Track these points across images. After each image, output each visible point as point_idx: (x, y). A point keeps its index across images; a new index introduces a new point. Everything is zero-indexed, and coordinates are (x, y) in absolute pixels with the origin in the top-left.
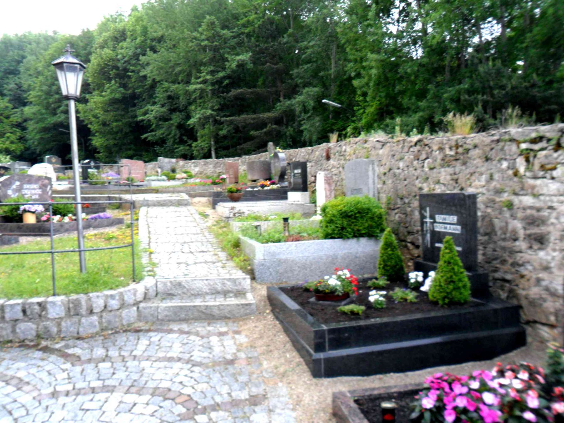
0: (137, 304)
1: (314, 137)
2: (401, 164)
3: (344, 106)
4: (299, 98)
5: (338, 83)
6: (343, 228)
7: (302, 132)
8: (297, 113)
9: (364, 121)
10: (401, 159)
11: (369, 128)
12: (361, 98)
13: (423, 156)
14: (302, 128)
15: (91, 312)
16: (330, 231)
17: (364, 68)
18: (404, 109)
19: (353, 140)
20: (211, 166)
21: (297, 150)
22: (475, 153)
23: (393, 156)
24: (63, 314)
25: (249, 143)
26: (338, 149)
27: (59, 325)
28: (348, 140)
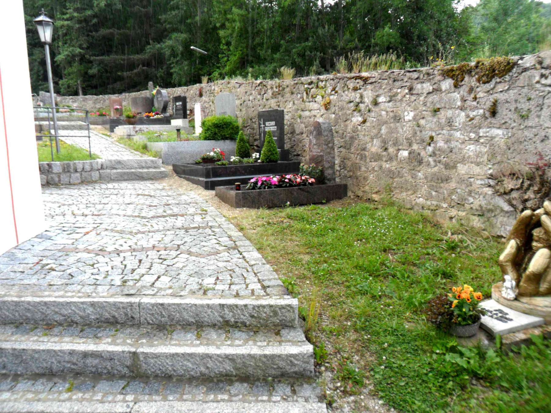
0: (98, 170)
1: (184, 80)
2: (251, 98)
3: (210, 53)
4: (169, 43)
5: (204, 31)
6: (215, 134)
7: (171, 74)
8: (166, 57)
9: (227, 68)
10: (251, 94)
11: (232, 73)
12: (225, 47)
13: (263, 92)
14: (172, 71)
15: (76, 171)
16: (207, 135)
17: (228, 20)
18: (262, 60)
19: (220, 82)
20: (91, 102)
21: (174, 89)
22: (287, 90)
23: (246, 92)
24: (61, 171)
25: (118, 83)
26: (209, 88)
27: (59, 177)
28: (216, 82)
